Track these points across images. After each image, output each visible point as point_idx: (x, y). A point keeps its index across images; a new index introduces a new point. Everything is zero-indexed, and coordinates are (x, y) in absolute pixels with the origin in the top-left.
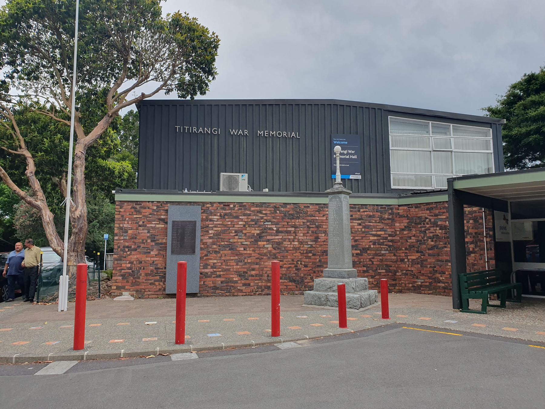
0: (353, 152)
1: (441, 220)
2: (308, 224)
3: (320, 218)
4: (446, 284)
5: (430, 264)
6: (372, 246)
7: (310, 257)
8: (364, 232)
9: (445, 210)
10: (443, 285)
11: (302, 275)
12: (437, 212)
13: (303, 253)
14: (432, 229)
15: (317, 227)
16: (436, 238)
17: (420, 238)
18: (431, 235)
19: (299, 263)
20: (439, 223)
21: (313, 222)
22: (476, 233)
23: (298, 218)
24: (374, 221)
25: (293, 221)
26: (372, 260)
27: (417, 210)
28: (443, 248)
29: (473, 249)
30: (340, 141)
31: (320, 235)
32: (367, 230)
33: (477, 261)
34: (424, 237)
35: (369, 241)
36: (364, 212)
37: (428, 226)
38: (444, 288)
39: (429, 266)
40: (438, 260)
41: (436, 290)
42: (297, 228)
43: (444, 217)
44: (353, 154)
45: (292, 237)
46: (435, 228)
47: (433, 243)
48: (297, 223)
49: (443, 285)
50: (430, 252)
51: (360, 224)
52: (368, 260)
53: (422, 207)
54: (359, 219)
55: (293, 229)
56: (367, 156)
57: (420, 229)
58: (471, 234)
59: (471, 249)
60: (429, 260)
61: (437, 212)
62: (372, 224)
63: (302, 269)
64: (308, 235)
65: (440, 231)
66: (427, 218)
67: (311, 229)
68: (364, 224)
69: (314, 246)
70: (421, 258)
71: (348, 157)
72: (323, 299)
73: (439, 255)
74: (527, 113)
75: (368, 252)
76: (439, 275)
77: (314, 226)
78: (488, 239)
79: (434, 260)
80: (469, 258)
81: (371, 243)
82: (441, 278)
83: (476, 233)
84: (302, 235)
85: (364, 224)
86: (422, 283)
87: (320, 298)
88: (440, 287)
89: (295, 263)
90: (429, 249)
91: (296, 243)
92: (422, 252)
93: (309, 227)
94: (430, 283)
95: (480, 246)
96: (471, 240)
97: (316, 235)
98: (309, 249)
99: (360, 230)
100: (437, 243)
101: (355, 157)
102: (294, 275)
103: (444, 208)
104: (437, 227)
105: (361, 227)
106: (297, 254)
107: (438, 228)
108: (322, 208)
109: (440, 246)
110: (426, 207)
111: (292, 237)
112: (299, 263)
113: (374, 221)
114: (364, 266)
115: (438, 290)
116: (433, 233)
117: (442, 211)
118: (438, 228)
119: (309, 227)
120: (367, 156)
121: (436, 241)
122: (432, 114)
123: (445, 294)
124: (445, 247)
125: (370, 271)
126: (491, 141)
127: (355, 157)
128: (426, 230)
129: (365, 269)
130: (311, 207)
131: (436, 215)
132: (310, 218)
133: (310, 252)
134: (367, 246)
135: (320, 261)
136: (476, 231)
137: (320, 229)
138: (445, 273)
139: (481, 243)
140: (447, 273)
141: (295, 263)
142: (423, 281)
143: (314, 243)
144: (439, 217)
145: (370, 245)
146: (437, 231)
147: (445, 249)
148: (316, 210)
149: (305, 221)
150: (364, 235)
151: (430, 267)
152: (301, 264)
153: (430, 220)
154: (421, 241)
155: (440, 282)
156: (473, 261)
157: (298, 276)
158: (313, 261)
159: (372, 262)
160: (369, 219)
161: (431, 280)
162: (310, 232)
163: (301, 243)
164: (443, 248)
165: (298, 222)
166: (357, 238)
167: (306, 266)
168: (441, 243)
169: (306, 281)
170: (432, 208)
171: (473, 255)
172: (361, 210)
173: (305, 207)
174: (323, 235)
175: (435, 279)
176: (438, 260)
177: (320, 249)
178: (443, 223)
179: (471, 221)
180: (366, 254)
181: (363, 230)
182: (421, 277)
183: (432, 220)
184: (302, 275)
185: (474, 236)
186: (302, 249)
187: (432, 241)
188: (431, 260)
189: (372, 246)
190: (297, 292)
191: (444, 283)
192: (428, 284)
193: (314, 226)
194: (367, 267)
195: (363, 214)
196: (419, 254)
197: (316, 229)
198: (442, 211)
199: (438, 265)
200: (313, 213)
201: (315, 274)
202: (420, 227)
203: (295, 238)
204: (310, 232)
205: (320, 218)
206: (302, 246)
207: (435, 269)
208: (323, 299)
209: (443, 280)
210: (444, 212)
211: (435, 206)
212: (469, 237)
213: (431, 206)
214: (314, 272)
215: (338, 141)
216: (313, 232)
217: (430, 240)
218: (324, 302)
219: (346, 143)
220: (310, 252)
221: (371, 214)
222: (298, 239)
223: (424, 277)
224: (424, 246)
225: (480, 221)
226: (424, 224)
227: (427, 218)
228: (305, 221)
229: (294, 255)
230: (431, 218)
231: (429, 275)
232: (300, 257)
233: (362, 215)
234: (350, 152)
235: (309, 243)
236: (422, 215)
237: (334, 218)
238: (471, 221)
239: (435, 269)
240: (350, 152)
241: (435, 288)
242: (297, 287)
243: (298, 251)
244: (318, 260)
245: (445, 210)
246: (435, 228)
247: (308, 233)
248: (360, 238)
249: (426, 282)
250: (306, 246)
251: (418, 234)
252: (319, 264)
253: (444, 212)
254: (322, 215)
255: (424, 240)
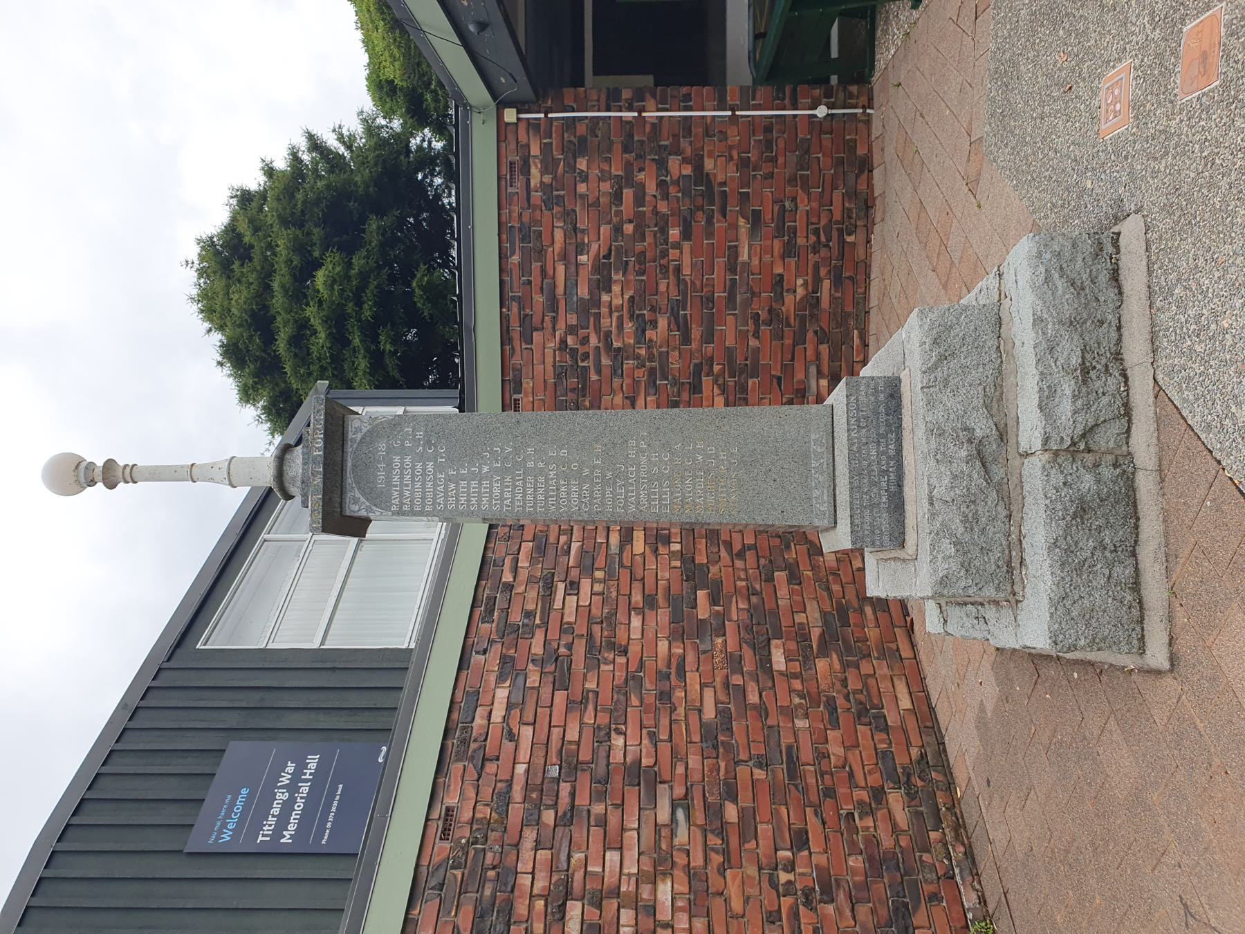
0: (291, 767)
1: (571, 284)
2: (549, 817)
3: (524, 754)
4: (823, 271)
5: (743, 336)
6: (676, 547)
7: (742, 813)
8: (610, 576)
9: (536, 266)
10: (826, 284)
11: (856, 862)
12: (539, 299)
13: (726, 853)
14: (605, 322)
15: (571, 767)
16: (640, 311)
17: (641, 374)
18: (629, 326)
19: (784, 877)
20: (583, 291)
21: (539, 792)
22: (626, 149)
23: (507, 876)
24: (563, 539)
25: (521, 909)
26: (737, 547)
27: (527, 384)
28: (679, 281)
29: (685, 161)
30: (228, 816)
31: (617, 756)
32: (601, 561)
33: (731, 147)
34: (638, 357)
35: (650, 557)
36: (515, 570)
37: (594, 341)
38: (838, 281)
39: (753, 343)
40: (731, 299)
41: (846, 316)
42: (567, 883)
43: (561, 269)
44: (301, 766)
45: (627, 916)
46: (604, 310)
47: (663, 322)
48: (540, 885)
49: (826, 284)
50: (696, 332)
51: (573, 587)
52: (739, 564)
53: (516, 360)
54: (549, 587)
55: (574, 910)
56: (324, 721)
57: (606, 372)
58: (628, 166)
59: (687, 170)
60: (730, 341)
61: (539, 299)
62: (575, 546)
63: (821, 859)
64: (613, 820)
65: (616, 289)
66: (564, 342)
67: (582, 800)
68: (574, 573)
69: (679, 791)
70: (722, 372)
71: (305, 789)
72: (1087, 482)
73: (711, 299)
74: (319, 359)
75: (701, 559)
76: (789, 298)
77: (565, 788)
78: (650, 103)
79: (730, 319)
80: (720, 178)
81: (662, 550)
82: (800, 292)
83: (626, 149)
84: (612, 857)
85: (574, 573)
86: (820, 374)
87: (1082, 510)
88: (833, 300)
89: (786, 902)
90: (686, 339)
91: (665, 891)
92: (698, 368)
93: (568, 818)
94: (822, 337)
95: (676, 136)
96: (651, 168)
97: (617, 780)
98: (699, 817)
99: (598, 588)
100: (663, 302)
101: (313, 762)
102: (863, 910)
103: (524, 268)
104: (598, 304)
105: (585, 584)
106: (734, 891)
107: (605, 298)
108: (465, 742)
109: (674, 294)
110: (517, 343)
111: (627, 916)
112: (784, 877)
113: (563, 539)
114: (770, 579)
115: (849, 309)
116: (620, 318)
117: (535, 278)
118: (605, 298)
119: (568, 818)
120: (324, 721)
121: (653, 309)
122: (238, 530)
123: (861, 277)
124: (678, 269)
125: (791, 555)
126: (368, 409)
127: (313, 762)
128: (609, 346)
129: (780, 576)
130: (451, 800)
131: (553, 304)
132: (516, 811)
133: (714, 812)
134: (678, 564)
135: (763, 763)
136: (618, 147)
137: (585, 755)
138: (781, 276)
139: (665, 132)
140: (778, 270)
141: (786, 902)
142: (813, 370)
143: (662, 789)
144: (560, 289)
145: (672, 554)
146: (617, 301)
147: (686, 270)
148: (472, 773)
149: (530, 835)
150: (625, 576)
151: (756, 335)
152: (790, 866)
153: (571, 330)
154: (652, 371)
155: (811, 301)
156: (732, 166)
157: (866, 886)
158: (765, 799)
159: (745, 548)
160: (551, 552)
161: (810, 335)
162: (598, 809)
163: (661, 863)
164: (679, 281)
165: (532, 873)
166: (637, 598)
167: (800, 840)
168: (662, 288)
169: (887, 842)
170: (524, 319)
171: (709, 164)
172: (507, 577)
173: (445, 835)
174: (618, 741)
175: (803, 319)
176: (731, 299)
177: (694, 761)
178: (584, 275)
179: (582, 164)
180: (714, 570)
181: (599, 574)
182: (799, 376)
183: (572, 319)
184: (856, 862)
185: (639, 157)
186: (697, 860)
187: (654, 324)
188: (728, 330)
189: (676, 547)
190: (970, 899)
191: (817, 281)
192: (824, 348)
193: (565, 788)
194: (772, 567)
195: (523, 575)
196: (706, 381)
197: (584, 781)
198: (535, 278)
199: (747, 303)
200: (486, 792)
201: (842, 790)
202: (599, 372)
203: (635, 903)
204: (598, 809)
205: (524, 754)
206: (680, 859)
207: (763, 315)
208: (1087, 482)
209: (805, 284)
210: (543, 270)
211: (515, 309)
212: (641, 176)
213: (516, 329)
214: (830, 792)
215: (224, 825)
216: (601, 796)
217: (649, 334)
218: (1107, 472)
219: (245, 791)
220: (714, 812)
221: (527, 547)
222: (639, 878)
223: (799, 366)
224: (675, 362)
225: (581, 129)
226: (586, 356)
227: (564, 342)
228: (530, 835)
229: (737, 905)
230: (561, 325)
231: (788, 341)
232: (752, 871)
233: (531, 580)
234: (285, 780)
235: (663, 815)
236: (549, 360)
237: (503, 472)
238: (582, 164)
239: (763, 315)
240: (285, 780)
241: (841, 319)
242: (934, 897)
243: (715, 882)
244: (759, 774)
245: (536, 266)
246: (604, 310)
247: (603, 822)
248: (637, 586)
249: (818, 355)
250: (682, 836)
251: (627, 381)
252: (781, 771)
253: (543, 270)
254: (508, 746)
255: (651, 358)
